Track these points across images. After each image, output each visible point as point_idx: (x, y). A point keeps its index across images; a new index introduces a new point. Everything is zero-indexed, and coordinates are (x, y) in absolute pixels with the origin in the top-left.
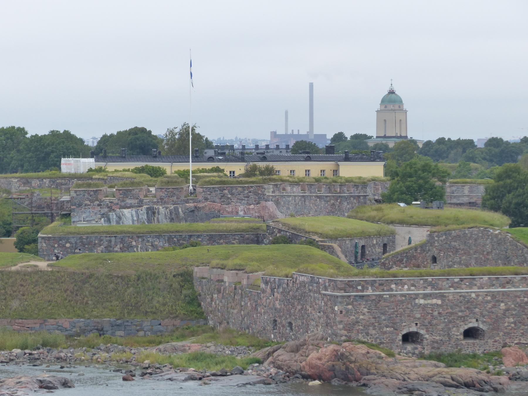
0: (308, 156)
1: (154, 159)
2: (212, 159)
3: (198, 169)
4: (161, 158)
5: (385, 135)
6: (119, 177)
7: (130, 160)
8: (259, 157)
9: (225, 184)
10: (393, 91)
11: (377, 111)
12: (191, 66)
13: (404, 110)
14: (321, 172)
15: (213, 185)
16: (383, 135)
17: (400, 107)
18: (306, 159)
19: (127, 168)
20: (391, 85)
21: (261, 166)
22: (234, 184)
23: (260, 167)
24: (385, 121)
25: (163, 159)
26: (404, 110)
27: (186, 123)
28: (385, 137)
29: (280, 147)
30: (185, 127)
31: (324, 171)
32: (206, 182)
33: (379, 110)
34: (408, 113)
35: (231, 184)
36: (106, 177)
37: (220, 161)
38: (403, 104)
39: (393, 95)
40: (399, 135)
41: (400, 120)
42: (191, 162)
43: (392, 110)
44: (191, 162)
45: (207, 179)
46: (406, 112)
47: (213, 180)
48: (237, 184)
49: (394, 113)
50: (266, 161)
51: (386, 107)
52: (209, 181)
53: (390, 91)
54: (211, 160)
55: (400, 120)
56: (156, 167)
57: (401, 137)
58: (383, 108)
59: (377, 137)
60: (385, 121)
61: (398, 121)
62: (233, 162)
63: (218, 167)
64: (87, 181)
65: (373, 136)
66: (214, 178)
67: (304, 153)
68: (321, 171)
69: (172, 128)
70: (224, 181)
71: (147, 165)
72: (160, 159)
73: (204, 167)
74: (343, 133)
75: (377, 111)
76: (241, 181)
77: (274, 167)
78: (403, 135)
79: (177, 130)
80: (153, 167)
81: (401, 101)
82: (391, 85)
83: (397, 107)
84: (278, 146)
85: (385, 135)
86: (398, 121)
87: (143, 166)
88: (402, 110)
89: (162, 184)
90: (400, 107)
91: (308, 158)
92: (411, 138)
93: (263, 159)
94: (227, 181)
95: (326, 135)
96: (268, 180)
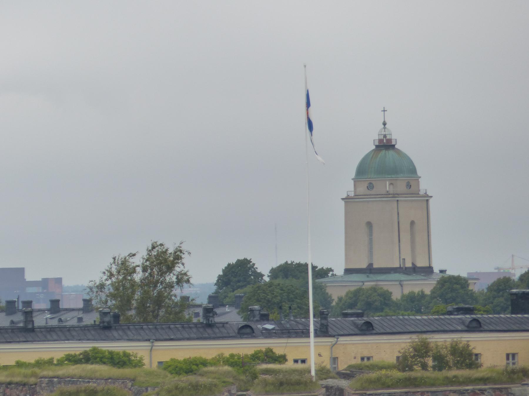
0: (475, 320)
1: (107, 333)
2: (248, 330)
3: (221, 356)
4: (123, 330)
5: (371, 265)
6: (80, 377)
7: (49, 337)
8: (354, 324)
9: (416, 386)
10: (390, 140)
11: (347, 200)
12: (308, 105)
13: (422, 193)
14: (508, 359)
15: (389, 387)
16: (364, 266)
17: (409, 186)
18: (468, 327)
19: (46, 357)
20: (385, 124)
21: (439, 344)
22: (440, 385)
23: (437, 346)
24: (369, 225)
25: (129, 333)
26: (422, 193)
27: (158, 243)
28: (370, 270)
29: (63, 305)
30: (154, 253)
31: (514, 355)
32: (371, 382)
33: (352, 194)
34: (431, 201)
35: (433, 385)
36: (32, 380)
37: (268, 334)
38: (417, 179)
39: (391, 153)
40: (409, 265)
41: (412, 223)
42: (312, 334)
43: (387, 194)
44: (312, 334)
45: (373, 375)
46: (427, 198)
47: (387, 377)
48: (447, 385)
49: (395, 204)
50: (372, 334)
51: (370, 187)
52: (378, 380)
53: (381, 141)
54: (247, 334)
55: (412, 223)
56: (118, 354)
57: (415, 270)
58: (362, 189)
59: (348, 271)
60: (369, 225)
61: (405, 226)
62: (301, 337)
63: (271, 351)
64: (87, 385)
65: (331, 270)
66: (389, 373)
67: (459, 310)
68: (508, 355)
69: (123, 254)
70: (415, 379)
71: (94, 349)
72: (121, 332)
73: (235, 352)
74: (250, 262)
75: (347, 200)
76: (455, 377)
77: (472, 345)
78: (421, 263)
79: (137, 261)
80: (111, 353)
81: (413, 171)
82: (385, 124)
83: (401, 187)
84: (87, 302)
85: (371, 265)
86: (405, 226)
87: (86, 352)
88: (416, 194)
89: (268, 389)
90: (409, 186)
91: (474, 324)
92: (442, 271)
93: (364, 328)
94: (422, 378)
95: (21, 271)
96: (521, 374)
